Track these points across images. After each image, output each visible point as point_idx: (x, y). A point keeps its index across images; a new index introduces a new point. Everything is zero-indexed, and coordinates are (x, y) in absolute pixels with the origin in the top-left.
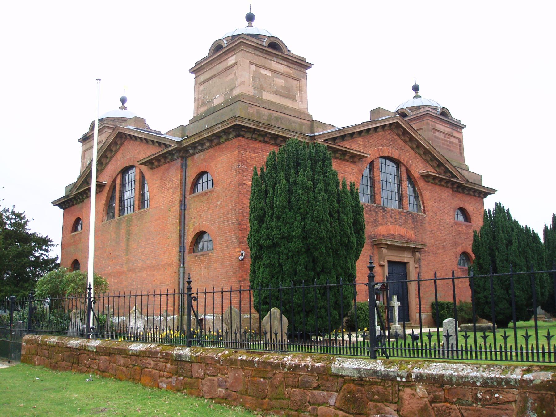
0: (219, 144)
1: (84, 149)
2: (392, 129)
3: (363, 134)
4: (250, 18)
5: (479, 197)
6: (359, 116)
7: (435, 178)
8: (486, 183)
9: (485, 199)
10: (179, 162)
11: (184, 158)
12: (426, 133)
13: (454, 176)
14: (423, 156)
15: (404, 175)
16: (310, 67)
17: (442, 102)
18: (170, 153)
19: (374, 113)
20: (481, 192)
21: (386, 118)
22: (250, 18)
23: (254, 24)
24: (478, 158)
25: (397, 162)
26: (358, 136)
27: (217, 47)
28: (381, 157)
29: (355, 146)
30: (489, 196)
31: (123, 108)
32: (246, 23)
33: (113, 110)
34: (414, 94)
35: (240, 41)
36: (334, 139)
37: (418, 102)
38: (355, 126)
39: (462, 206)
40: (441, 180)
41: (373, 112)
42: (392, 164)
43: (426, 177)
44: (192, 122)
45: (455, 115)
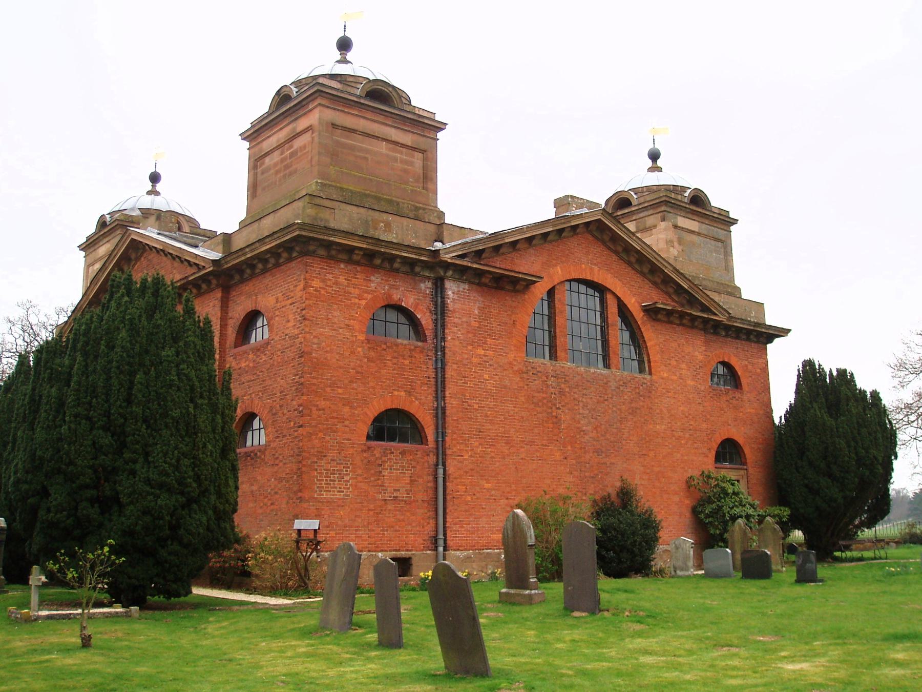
0: (277, 265)
1: (90, 260)
2: (590, 232)
3: (550, 237)
4: (344, 45)
5: (758, 342)
6: (538, 210)
7: (669, 313)
8: (771, 319)
9: (769, 346)
10: (219, 294)
11: (227, 290)
12: (659, 238)
13: (705, 309)
14: (650, 277)
15: (613, 308)
16: (442, 129)
17: (690, 181)
18: (205, 278)
19: (560, 203)
20: (759, 335)
21: (460, 242)
22: (344, 45)
23: (350, 56)
24: (757, 275)
25: (600, 289)
26: (542, 242)
27: (282, 97)
28: (570, 281)
29: (525, 264)
30: (777, 340)
31: (153, 192)
32: (337, 55)
33: (131, 196)
34: (649, 163)
35: (315, 89)
36: (479, 254)
37: (654, 179)
38: (519, 230)
39: (365, 428)
40: (682, 315)
41: (560, 203)
42: (590, 291)
43: (652, 312)
44: (244, 225)
45: (716, 201)
